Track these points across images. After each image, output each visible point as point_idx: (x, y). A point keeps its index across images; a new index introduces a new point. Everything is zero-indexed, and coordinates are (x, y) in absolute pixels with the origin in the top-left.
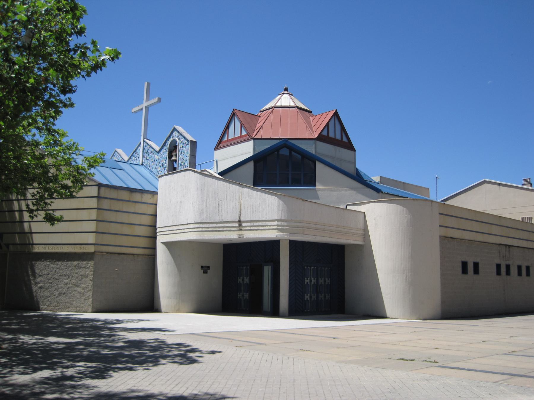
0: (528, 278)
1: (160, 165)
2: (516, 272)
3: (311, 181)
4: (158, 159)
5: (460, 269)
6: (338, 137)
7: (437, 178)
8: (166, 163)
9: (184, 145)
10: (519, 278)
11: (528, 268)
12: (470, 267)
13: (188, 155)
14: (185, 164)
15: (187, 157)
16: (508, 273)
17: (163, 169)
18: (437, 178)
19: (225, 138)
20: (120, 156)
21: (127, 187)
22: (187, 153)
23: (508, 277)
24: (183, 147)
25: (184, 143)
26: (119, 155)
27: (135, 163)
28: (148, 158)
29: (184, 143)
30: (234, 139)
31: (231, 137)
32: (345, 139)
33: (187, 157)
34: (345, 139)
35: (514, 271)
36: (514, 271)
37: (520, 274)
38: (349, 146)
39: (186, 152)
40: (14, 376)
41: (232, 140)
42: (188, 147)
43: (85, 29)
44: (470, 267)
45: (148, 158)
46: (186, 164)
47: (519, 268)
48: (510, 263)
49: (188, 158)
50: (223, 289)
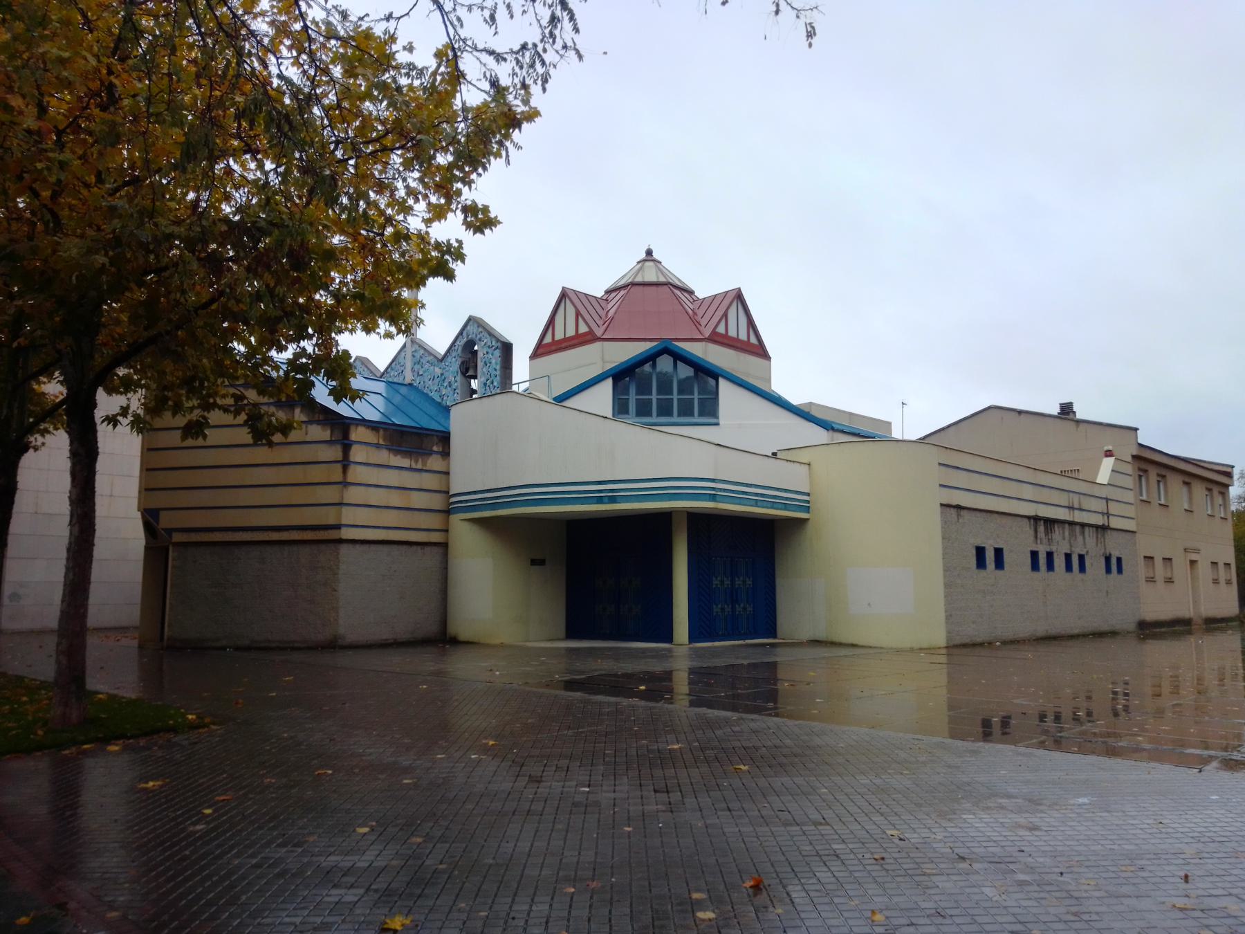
0: (1081, 576)
1: (445, 384)
2: (1063, 565)
3: (709, 410)
4: (442, 374)
5: (973, 561)
6: (743, 336)
7: (903, 404)
8: (456, 381)
9: (490, 350)
10: (1068, 575)
11: (1081, 558)
12: (990, 556)
13: (498, 367)
14: (493, 383)
15: (496, 370)
16: (1050, 566)
17: (452, 393)
18: (903, 404)
19: (682, 349)
20: (366, 369)
21: (413, 424)
22: (496, 364)
23: (1051, 573)
24: (487, 353)
25: (489, 347)
26: (363, 367)
27: (395, 380)
28: (421, 373)
29: (489, 347)
30: (565, 340)
31: (559, 335)
32: (753, 340)
33: (496, 370)
34: (753, 340)
35: (1059, 562)
36: (1059, 562)
37: (1069, 567)
38: (760, 351)
39: (493, 361)
40: (1030, 528)
41: (560, 341)
42: (497, 353)
43: (488, 207)
44: (990, 556)
45: (421, 373)
46: (495, 384)
47: (1068, 557)
48: (1054, 548)
49: (498, 373)
50: (774, 570)
